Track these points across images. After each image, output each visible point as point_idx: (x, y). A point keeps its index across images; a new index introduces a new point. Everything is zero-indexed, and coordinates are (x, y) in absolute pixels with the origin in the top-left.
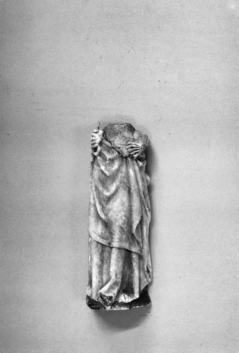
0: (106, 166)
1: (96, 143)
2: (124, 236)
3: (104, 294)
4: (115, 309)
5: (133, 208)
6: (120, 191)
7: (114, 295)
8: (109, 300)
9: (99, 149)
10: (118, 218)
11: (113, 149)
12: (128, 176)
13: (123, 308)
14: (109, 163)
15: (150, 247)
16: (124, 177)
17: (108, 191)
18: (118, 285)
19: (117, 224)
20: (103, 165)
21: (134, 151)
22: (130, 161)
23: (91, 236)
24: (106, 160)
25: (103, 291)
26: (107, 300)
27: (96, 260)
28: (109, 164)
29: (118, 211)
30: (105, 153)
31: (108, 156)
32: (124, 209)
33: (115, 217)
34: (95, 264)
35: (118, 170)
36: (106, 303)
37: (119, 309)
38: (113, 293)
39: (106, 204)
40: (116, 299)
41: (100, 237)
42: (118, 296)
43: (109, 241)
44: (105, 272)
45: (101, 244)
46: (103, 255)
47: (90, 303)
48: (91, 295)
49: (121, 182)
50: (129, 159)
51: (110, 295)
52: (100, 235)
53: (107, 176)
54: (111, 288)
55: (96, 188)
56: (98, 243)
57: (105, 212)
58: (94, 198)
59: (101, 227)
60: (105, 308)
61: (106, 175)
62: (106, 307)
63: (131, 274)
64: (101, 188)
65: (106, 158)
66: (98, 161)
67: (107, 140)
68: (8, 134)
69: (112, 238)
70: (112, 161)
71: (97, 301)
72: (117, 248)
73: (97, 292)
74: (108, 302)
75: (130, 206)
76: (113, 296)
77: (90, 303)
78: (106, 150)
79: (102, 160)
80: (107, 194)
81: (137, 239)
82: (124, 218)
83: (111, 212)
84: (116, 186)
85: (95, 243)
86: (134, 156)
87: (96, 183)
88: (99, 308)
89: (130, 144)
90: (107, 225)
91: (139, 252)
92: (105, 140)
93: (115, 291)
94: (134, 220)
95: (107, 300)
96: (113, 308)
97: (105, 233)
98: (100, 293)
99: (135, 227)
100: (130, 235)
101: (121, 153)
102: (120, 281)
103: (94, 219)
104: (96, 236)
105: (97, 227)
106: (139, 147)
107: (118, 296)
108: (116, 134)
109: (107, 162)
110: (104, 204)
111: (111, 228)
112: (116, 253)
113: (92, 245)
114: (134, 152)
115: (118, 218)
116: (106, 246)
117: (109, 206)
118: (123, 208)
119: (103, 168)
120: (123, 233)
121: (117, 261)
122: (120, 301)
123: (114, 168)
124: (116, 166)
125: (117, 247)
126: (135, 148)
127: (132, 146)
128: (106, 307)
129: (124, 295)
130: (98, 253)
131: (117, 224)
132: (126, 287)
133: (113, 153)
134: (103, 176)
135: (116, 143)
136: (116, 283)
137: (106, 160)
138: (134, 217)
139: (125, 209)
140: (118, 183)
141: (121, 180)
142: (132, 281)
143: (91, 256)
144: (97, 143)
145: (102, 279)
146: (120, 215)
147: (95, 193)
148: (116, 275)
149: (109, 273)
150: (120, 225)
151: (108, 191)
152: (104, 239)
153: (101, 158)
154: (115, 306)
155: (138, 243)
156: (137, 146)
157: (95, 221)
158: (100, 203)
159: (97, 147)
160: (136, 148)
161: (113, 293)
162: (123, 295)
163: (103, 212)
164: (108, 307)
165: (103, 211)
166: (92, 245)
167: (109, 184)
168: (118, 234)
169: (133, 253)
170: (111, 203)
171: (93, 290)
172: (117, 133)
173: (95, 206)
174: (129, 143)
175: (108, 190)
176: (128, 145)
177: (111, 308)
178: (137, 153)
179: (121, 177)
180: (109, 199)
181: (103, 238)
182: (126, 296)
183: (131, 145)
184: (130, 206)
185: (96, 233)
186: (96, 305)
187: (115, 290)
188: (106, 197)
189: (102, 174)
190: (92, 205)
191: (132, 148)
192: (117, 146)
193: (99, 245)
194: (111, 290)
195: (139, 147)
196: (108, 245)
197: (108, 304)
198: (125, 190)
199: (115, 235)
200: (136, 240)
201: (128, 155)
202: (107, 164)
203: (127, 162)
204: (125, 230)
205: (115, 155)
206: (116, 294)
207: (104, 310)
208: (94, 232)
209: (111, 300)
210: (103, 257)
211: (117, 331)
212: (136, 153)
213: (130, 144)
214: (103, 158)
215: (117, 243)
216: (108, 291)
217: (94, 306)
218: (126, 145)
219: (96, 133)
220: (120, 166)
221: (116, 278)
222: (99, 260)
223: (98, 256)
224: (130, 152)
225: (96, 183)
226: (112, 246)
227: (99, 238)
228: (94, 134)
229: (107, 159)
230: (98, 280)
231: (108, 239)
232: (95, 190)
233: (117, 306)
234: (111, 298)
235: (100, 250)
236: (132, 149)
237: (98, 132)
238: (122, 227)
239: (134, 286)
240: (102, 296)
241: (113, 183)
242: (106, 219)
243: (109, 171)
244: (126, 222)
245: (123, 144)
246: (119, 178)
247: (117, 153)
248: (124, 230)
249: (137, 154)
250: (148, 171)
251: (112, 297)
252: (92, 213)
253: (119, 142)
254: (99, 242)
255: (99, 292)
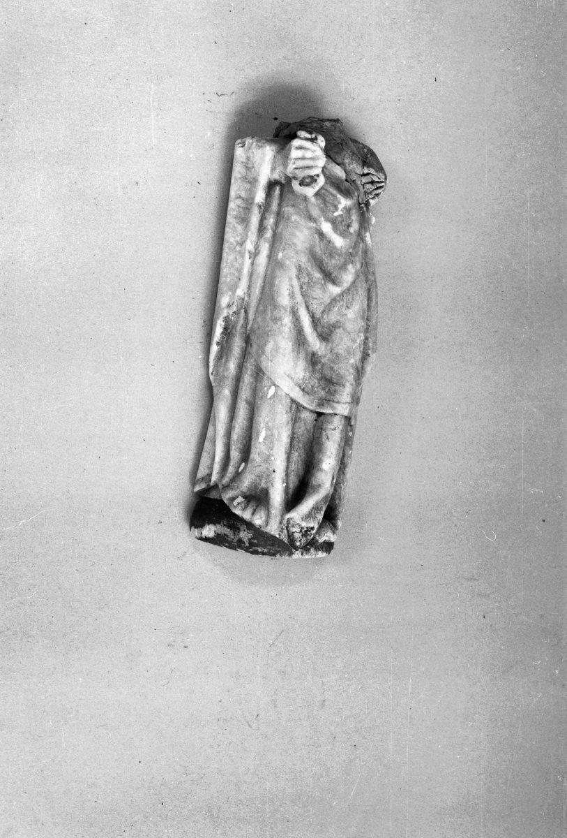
10: (354, 347)
15: (369, 298)
41: (300, 387)
56: (293, 401)
58: (292, 295)
59: (304, 363)
84: (356, 271)
89: (368, 174)
115: (354, 347)
157: (293, 351)
163: (317, 331)
168: (352, 385)
173: (294, 313)
190: (288, 310)
208: (288, 376)
211: (315, 478)
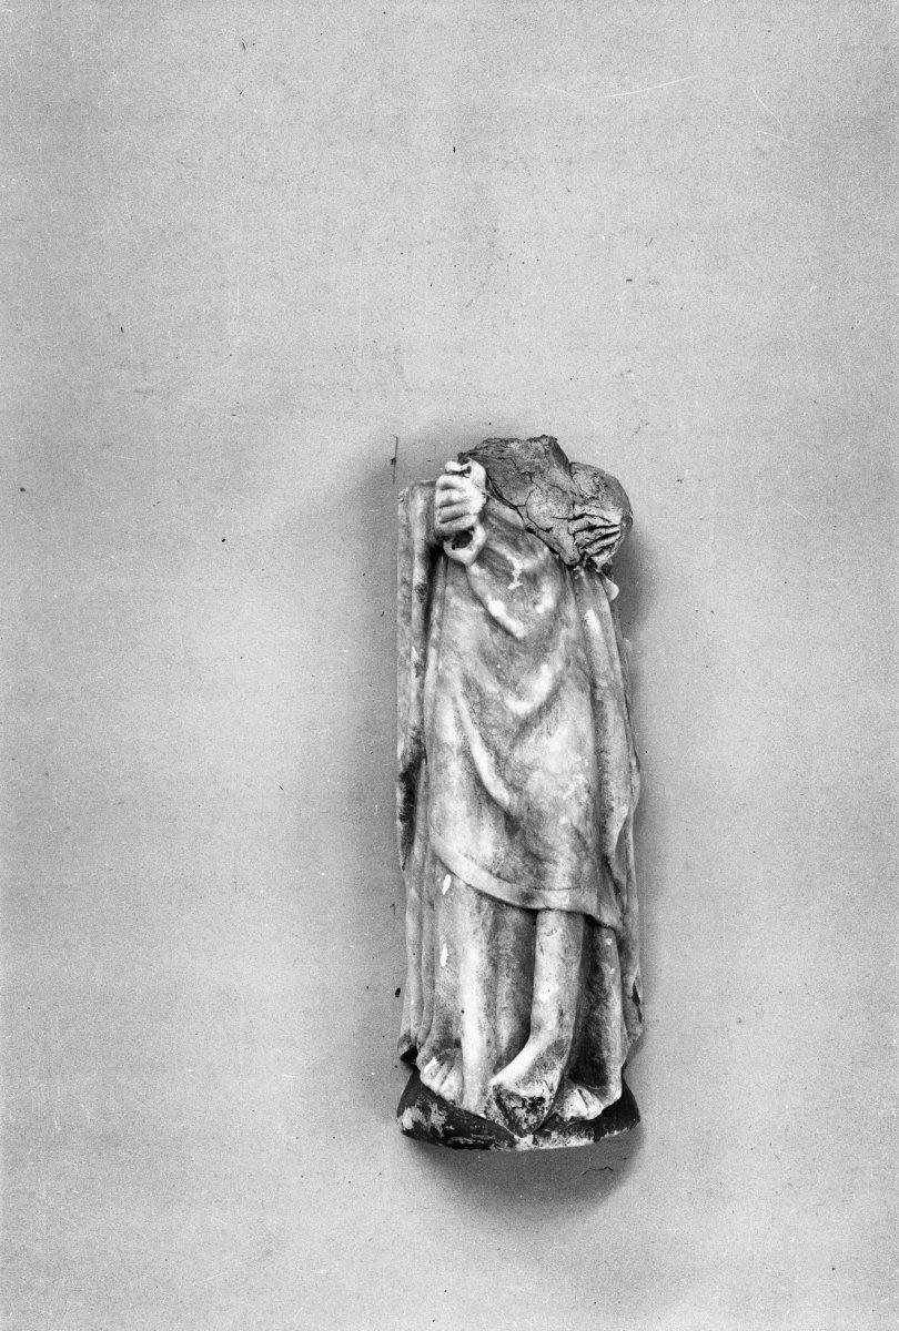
0: (508, 598)
1: (468, 514)
2: (586, 867)
3: (513, 1089)
4: (546, 1146)
5: (608, 758)
6: (564, 695)
7: (551, 1090)
8: (528, 1112)
9: (480, 536)
11: (530, 537)
12: (585, 639)
13: (575, 1142)
14: (521, 587)
16: (577, 643)
17: (520, 698)
18: (562, 1054)
19: (564, 820)
20: (495, 598)
21: (596, 541)
22: (585, 580)
23: (453, 869)
24: (511, 578)
25: (510, 1076)
26: (521, 1113)
27: (478, 962)
28: (521, 594)
29: (564, 772)
30: (503, 549)
31: (520, 564)
32: (582, 762)
33: (556, 793)
34: (474, 976)
35: (556, 615)
36: (514, 1124)
37: (561, 1146)
38: (544, 1088)
39: (512, 747)
40: (553, 1106)
41: (491, 872)
42: (560, 1095)
43: (524, 886)
44: (505, 1005)
45: (492, 899)
46: (497, 940)
47: (451, 1127)
48: (461, 1095)
49: (568, 662)
50: (583, 573)
51: (537, 1090)
52: (489, 863)
53: (516, 640)
54: (541, 1064)
55: (469, 684)
56: (481, 894)
57: (509, 775)
58: (460, 725)
60: (513, 1143)
61: (508, 633)
62: (516, 1137)
63: (593, 1008)
64: (491, 687)
65: (512, 568)
66: (473, 580)
67: (500, 498)
68: (22, 490)
69: (540, 876)
70: (531, 579)
71: (483, 1115)
72: (562, 911)
73: (485, 1081)
74: (526, 1120)
75: (599, 752)
76: (547, 1095)
77: (451, 1127)
78: (505, 539)
79: (489, 577)
80: (521, 708)
81: (616, 876)
82: (585, 797)
83: (536, 775)
85: (472, 895)
86: (596, 559)
87: (470, 666)
88: (491, 1142)
89: (581, 516)
90: (517, 826)
91: (620, 926)
92: (496, 502)
93: (554, 1077)
94: (614, 804)
95: (521, 1113)
96: (541, 1140)
97: (507, 855)
98: (498, 1089)
99: (615, 831)
100: (606, 867)
101: (556, 548)
102: (571, 1036)
103: (464, 803)
104: (476, 867)
105: (477, 838)
106: (612, 526)
107: (560, 1095)
108: (526, 477)
109: (512, 586)
110: (504, 747)
111: (536, 835)
112: (560, 930)
113: (460, 906)
114: (596, 546)
116: (508, 904)
117: (526, 753)
118: (580, 758)
119: (497, 608)
120: (584, 853)
121: (564, 960)
122: (569, 1114)
123: (540, 609)
124: (547, 598)
125: (565, 907)
126: (600, 530)
127: (590, 520)
128: (516, 1137)
129: (580, 1092)
130: (481, 933)
131: (564, 820)
132: (585, 1066)
133: (532, 549)
134: (497, 638)
135: (535, 510)
136: (557, 1046)
137: (511, 578)
138: (613, 792)
139: (587, 764)
140: (559, 665)
141: (568, 655)
142: (599, 1035)
143: (451, 945)
144: (472, 512)
145: (494, 1031)
146: (572, 787)
147: (463, 704)
148: (562, 1014)
149: (530, 1005)
150: (575, 824)
151: (520, 696)
152: (504, 879)
153: (484, 571)
154: (549, 1134)
155: (617, 889)
156: (607, 524)
157: (470, 814)
158: (487, 743)
159: (472, 529)
160: (604, 531)
161: (544, 1088)
162: (576, 1091)
163: (503, 777)
164: (525, 1139)
165: (501, 773)
166: (460, 906)
167: (522, 672)
169: (604, 932)
170: (532, 740)
171: (467, 1078)
172: (531, 475)
173: (466, 754)
174: (578, 510)
175: (519, 693)
176: (575, 518)
177: (535, 1141)
178: (608, 547)
179: (566, 643)
180: (525, 725)
181: (498, 876)
182: (586, 1092)
183: (587, 519)
184: (599, 752)
185: (474, 856)
186: (479, 1131)
187: (555, 1071)
188: (516, 718)
189: (493, 631)
190: (454, 750)
191: (591, 528)
192: (541, 524)
193: (485, 904)
194: (537, 1073)
195: (612, 526)
196: (518, 903)
197: (525, 1127)
198: (582, 690)
199: (555, 863)
200: (612, 878)
201: (578, 557)
202: (513, 592)
203: (576, 582)
204: (589, 841)
205: (541, 556)
206: (556, 1088)
207: (509, 1150)
208: (466, 856)
209: (536, 1111)
210: (498, 948)
212: (603, 549)
213: (581, 516)
214: (493, 570)
215: (565, 893)
216: (529, 1078)
217: (469, 1137)
218: (570, 520)
219: (462, 474)
220: (561, 599)
221: (561, 1026)
222: (485, 961)
223: (484, 946)
224: (584, 547)
225: (470, 666)
226: (538, 905)
227: (488, 874)
228: (455, 480)
229: (516, 574)
230: (485, 1036)
231: (520, 878)
232: (464, 694)
233: (554, 1135)
234: (536, 1103)
235: (489, 923)
236: (591, 536)
237: (469, 470)
238: (582, 831)
239: (605, 1053)
240: (501, 1096)
241: (537, 664)
242: (516, 803)
243: (523, 618)
244: (591, 811)
245: (557, 515)
246: (562, 645)
247: (546, 549)
248: (585, 843)
249: (606, 553)
250: (626, 613)
251: (542, 1099)
252: (454, 781)
253: (544, 508)
254: (486, 891)
255: (494, 1081)
